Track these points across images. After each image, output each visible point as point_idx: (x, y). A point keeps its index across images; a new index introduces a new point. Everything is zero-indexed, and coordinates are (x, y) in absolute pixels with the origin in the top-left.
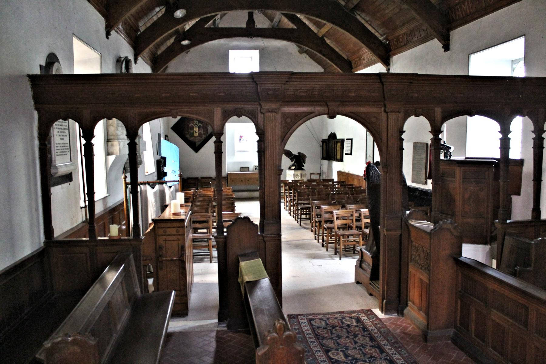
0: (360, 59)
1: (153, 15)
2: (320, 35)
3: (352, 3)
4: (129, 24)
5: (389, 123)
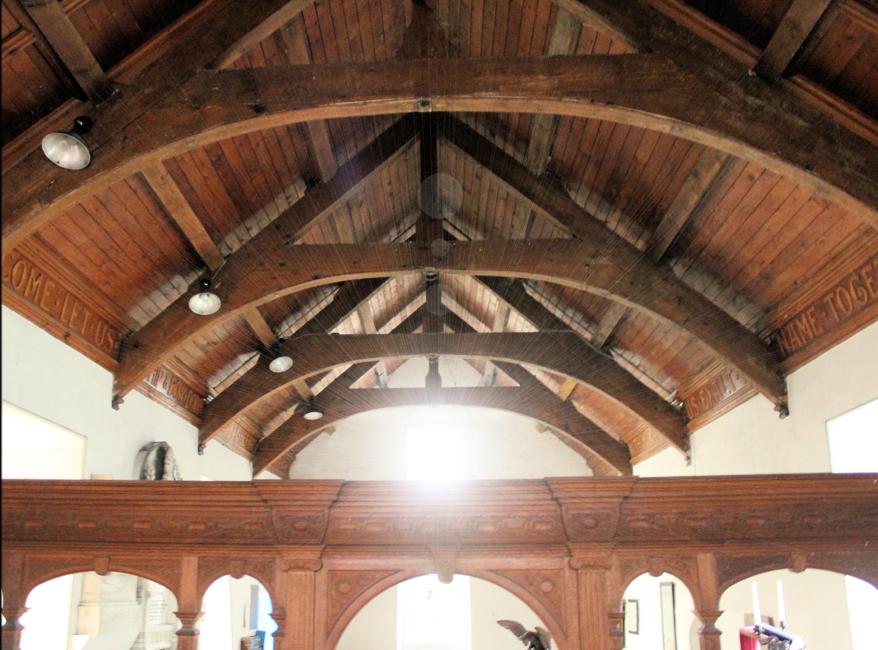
0: (640, 439)
1: (236, 368)
2: (564, 397)
3: (602, 336)
4: (186, 385)
5: (582, 595)
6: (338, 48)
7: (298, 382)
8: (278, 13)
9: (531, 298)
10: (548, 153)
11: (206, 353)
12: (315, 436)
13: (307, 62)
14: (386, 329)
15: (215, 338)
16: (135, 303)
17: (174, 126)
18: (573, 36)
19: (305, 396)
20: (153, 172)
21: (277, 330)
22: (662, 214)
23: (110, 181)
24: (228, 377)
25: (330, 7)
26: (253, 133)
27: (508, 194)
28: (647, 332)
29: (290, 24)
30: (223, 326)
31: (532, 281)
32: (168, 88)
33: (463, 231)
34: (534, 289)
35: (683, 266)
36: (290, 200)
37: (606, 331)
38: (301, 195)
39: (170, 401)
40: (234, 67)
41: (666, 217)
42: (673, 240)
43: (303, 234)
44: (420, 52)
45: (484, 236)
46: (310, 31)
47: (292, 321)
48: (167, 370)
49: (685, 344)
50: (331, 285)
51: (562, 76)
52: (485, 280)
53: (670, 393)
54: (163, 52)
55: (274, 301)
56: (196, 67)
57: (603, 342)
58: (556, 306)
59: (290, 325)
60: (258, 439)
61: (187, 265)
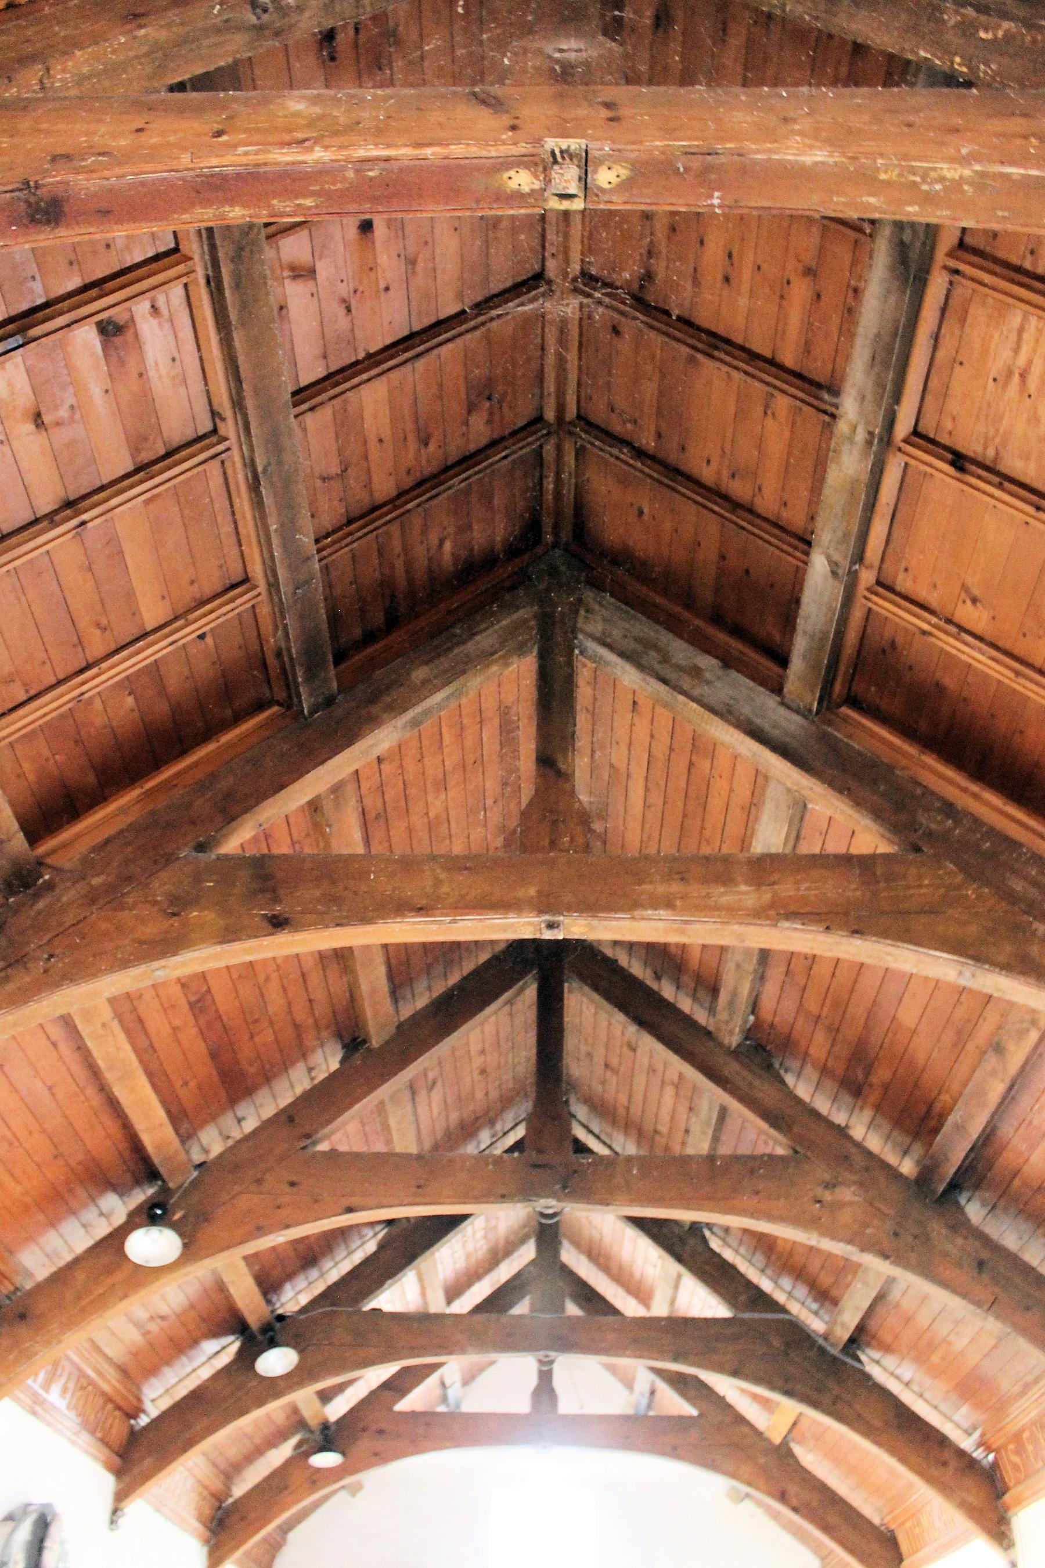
1: (196, 1364)
4: (103, 1394)
6: (410, 830)
7: (304, 1397)
8: (321, 771)
9: (719, 1256)
10: (750, 1009)
11: (146, 1333)
12: (326, 1498)
13: (360, 850)
14: (463, 1305)
15: (164, 1309)
16: (30, 1238)
17: (134, 941)
18: (790, 826)
19: (314, 1423)
20: (88, 1015)
21: (274, 1299)
22: (942, 1117)
23: (15, 1025)
24: (180, 1380)
25: (401, 766)
26: (265, 961)
27: (681, 1075)
28: (923, 1319)
29: (337, 789)
30: (180, 1287)
31: (721, 1227)
32: (129, 879)
33: (603, 1137)
34: (724, 1240)
35: (984, 1205)
36: (313, 1074)
37: (849, 1319)
38: (334, 1065)
39: (70, 1420)
40: (240, 852)
41: (950, 1119)
42: (963, 1161)
43: (332, 1133)
44: (546, 842)
45: (639, 1145)
46: (368, 802)
47: (301, 1282)
48: (73, 1363)
49: (992, 1342)
50: (372, 1224)
51: (776, 887)
52: (639, 1223)
53: (970, 1435)
54: (130, 819)
55: (274, 1249)
56: (178, 849)
57: (846, 1336)
58: (763, 1271)
59: (298, 1289)
60: (221, 1502)
61: (128, 1176)
